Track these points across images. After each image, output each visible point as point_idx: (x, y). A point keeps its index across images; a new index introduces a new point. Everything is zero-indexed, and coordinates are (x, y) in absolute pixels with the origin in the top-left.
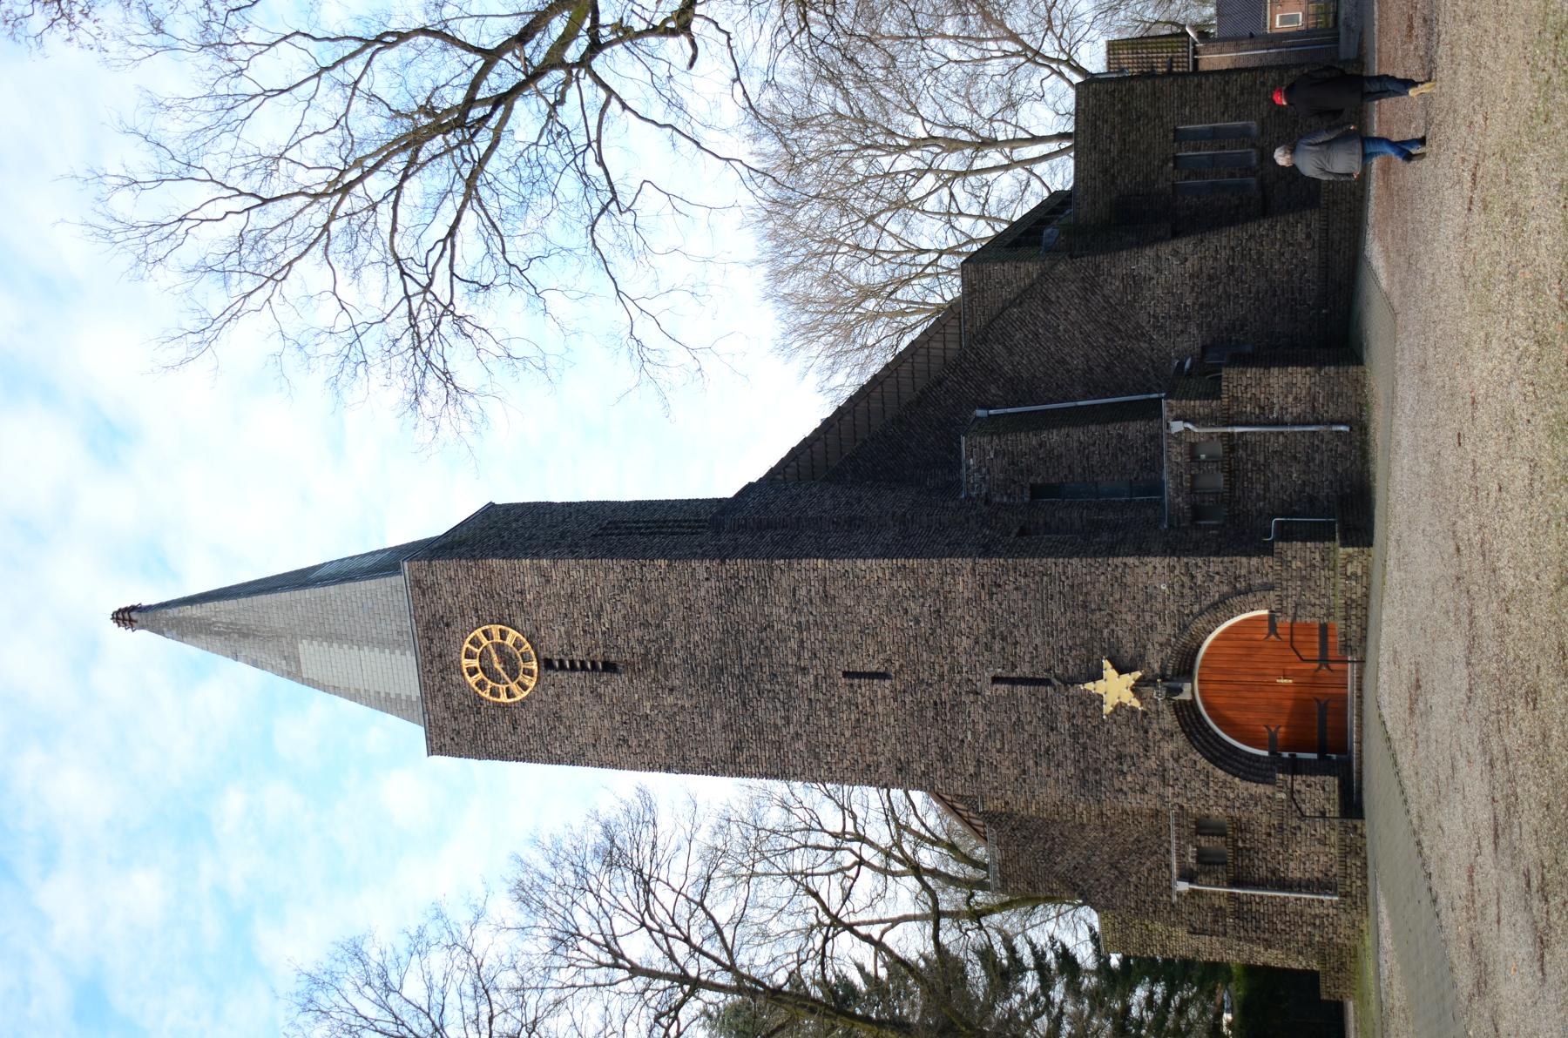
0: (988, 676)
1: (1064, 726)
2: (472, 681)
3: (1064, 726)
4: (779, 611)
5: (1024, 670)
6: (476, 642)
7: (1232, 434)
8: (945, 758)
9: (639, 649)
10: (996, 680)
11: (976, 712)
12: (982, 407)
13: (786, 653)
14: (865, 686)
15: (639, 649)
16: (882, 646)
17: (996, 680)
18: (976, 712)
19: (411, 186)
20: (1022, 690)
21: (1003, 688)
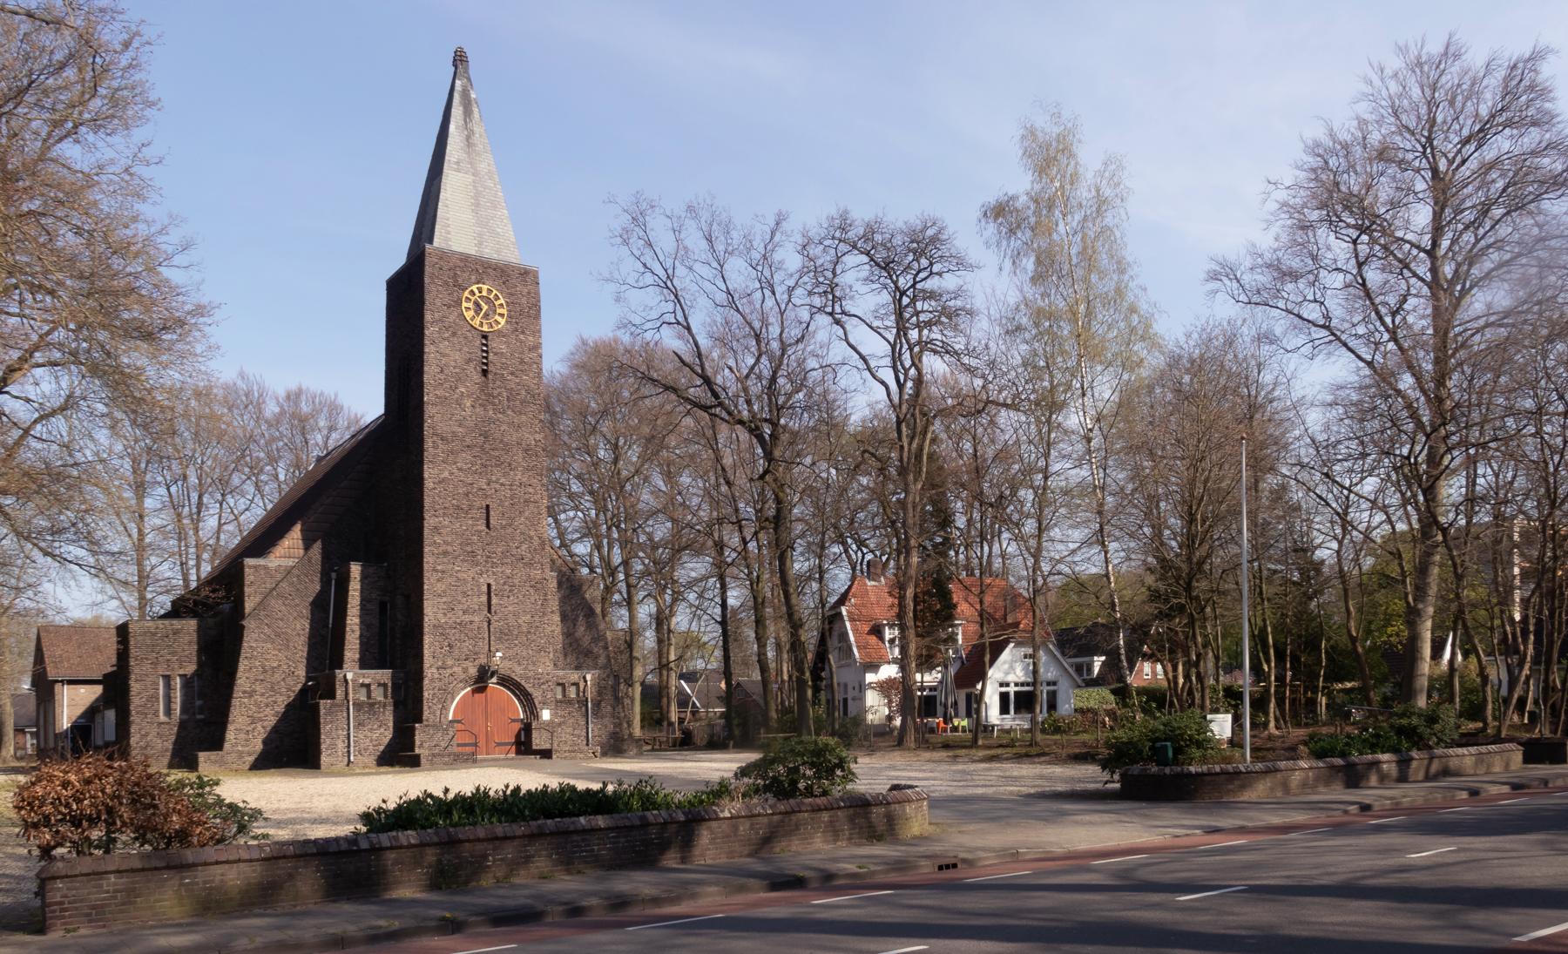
0: (491, 582)
1: (467, 618)
2: (502, 301)
3: (467, 618)
4: (519, 476)
5: (494, 601)
6: (472, 293)
7: (1240, 600)
8: (445, 553)
9: (496, 393)
10: (489, 586)
11: (472, 573)
12: (1506, 601)
13: (497, 474)
14: (482, 514)
15: (496, 393)
16: (503, 527)
17: (489, 586)
18: (472, 573)
19: (778, 331)
20: (484, 598)
21: (485, 588)
